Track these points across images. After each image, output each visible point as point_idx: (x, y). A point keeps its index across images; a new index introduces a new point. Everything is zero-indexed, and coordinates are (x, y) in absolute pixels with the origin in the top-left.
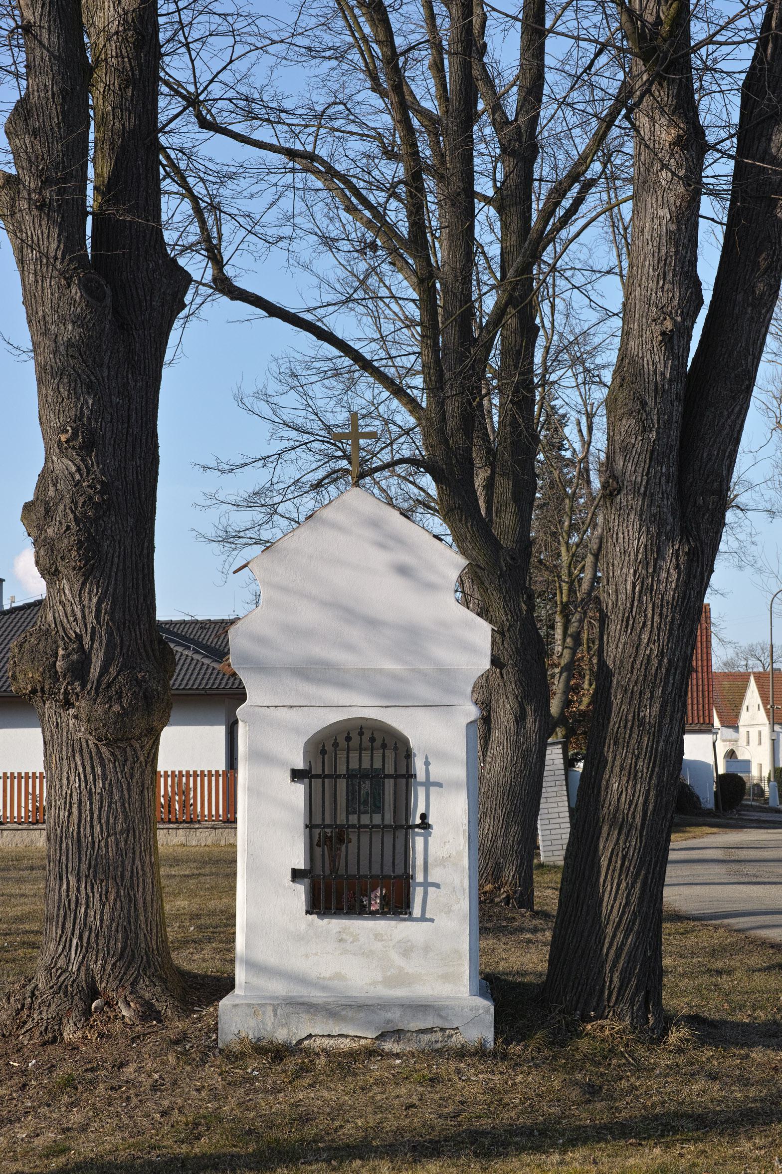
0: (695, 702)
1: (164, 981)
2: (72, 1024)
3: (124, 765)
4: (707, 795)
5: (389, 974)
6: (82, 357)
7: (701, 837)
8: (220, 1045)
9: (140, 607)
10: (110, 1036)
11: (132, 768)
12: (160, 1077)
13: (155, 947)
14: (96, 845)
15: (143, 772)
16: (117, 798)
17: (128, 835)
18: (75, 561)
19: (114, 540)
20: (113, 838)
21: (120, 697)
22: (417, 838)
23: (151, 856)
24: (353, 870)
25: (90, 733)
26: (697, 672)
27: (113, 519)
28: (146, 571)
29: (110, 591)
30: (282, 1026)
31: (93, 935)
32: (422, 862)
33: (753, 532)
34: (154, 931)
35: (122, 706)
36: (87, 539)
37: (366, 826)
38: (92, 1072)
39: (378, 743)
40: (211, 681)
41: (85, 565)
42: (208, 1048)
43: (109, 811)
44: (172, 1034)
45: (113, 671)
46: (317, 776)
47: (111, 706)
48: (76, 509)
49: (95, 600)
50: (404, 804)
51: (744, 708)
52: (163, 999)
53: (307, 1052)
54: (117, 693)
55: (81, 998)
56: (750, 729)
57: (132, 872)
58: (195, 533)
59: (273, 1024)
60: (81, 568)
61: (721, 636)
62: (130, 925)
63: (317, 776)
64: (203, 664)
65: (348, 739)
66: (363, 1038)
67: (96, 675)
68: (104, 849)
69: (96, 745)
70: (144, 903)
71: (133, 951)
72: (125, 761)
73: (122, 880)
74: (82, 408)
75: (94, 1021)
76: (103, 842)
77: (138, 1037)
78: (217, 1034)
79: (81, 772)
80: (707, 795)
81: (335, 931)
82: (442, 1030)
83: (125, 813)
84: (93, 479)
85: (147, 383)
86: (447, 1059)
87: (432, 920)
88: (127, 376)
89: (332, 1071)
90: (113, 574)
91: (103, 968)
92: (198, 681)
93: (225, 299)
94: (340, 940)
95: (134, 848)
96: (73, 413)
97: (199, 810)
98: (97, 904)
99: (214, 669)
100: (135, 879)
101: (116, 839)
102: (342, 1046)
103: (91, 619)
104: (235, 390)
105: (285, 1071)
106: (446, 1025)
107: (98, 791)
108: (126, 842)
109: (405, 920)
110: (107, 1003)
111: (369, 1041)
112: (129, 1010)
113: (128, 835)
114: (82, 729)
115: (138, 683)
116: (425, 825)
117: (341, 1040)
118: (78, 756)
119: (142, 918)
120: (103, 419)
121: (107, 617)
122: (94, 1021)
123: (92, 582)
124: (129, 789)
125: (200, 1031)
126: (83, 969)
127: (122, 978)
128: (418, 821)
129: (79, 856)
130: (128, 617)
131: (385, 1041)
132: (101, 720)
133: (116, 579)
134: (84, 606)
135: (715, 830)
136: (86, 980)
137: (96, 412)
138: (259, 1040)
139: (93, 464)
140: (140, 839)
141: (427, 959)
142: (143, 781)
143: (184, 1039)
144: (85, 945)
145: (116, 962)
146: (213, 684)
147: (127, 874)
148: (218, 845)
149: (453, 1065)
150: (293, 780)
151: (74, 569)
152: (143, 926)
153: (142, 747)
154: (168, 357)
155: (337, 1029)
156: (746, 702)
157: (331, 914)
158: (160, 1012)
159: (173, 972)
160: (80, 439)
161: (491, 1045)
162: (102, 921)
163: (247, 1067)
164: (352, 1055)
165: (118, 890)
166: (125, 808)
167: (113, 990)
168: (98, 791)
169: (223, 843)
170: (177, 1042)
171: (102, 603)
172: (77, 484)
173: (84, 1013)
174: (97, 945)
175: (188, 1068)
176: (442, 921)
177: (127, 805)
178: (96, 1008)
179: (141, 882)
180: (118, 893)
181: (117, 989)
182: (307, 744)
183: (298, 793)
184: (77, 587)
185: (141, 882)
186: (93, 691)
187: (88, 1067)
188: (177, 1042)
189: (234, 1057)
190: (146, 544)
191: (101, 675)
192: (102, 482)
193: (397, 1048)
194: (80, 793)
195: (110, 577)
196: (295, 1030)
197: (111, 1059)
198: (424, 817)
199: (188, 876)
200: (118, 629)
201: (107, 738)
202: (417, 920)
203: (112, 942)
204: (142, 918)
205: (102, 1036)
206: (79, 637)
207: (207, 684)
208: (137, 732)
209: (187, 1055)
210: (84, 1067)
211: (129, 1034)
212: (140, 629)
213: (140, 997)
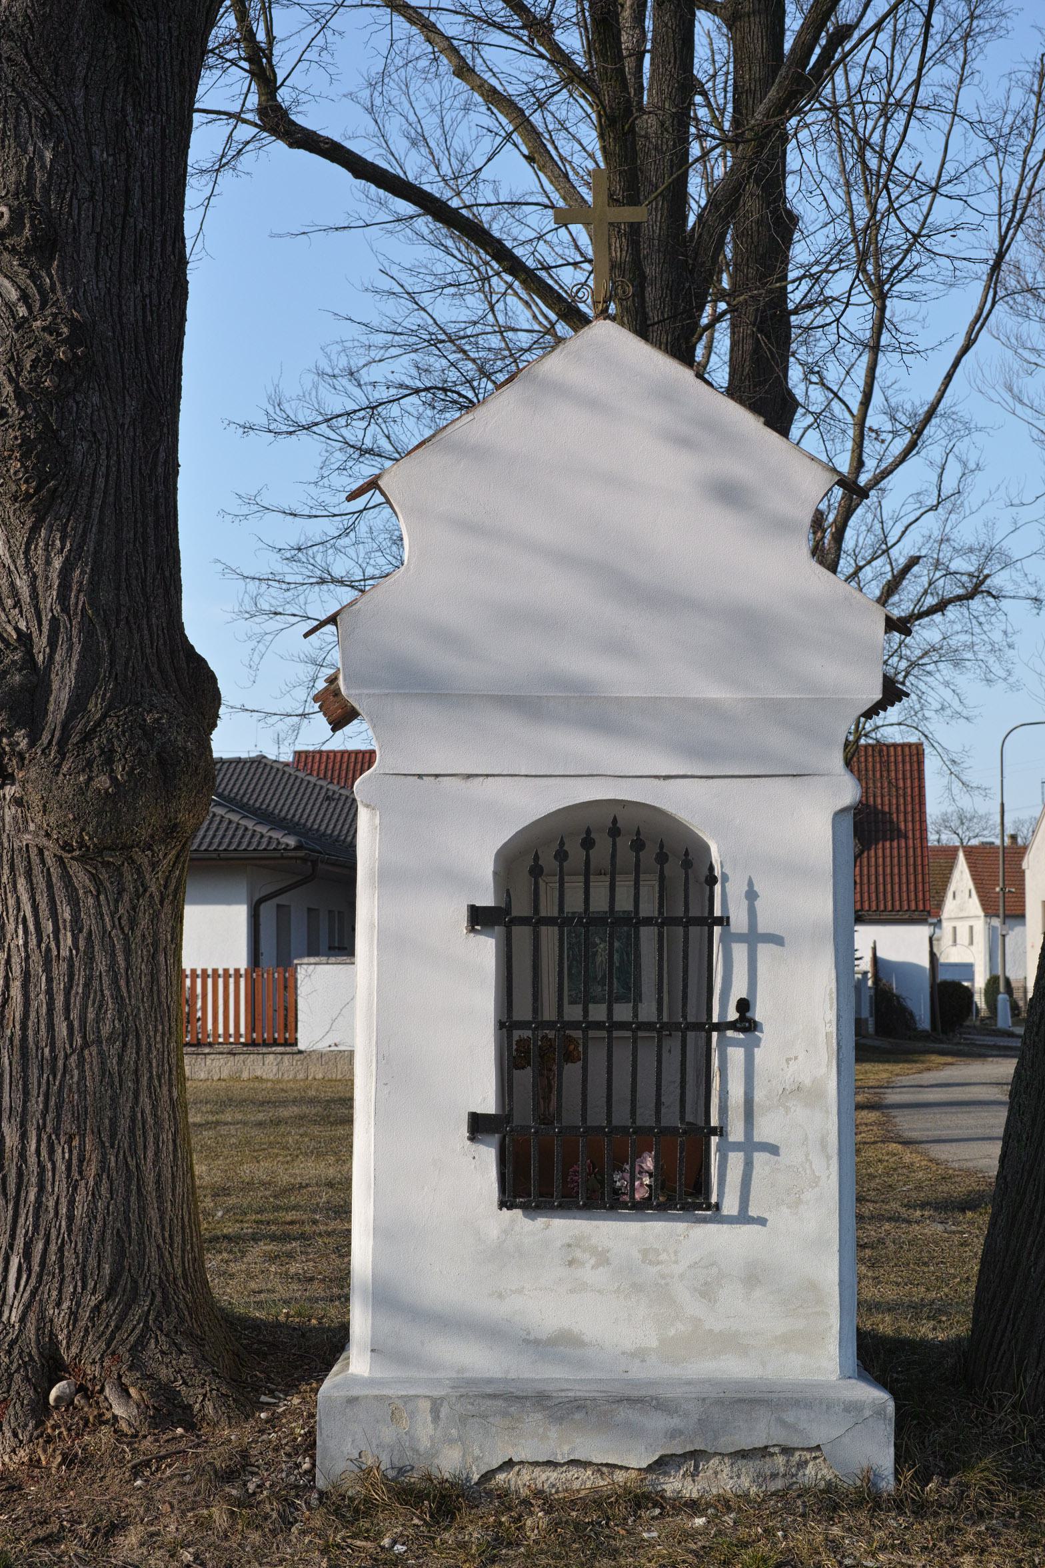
0: (904, 880)
1: (198, 1341)
2: (8, 1434)
3: (117, 901)
4: (922, 1010)
5: (672, 1332)
6: (30, 61)
7: (937, 1069)
8: (321, 1483)
9: (149, 580)
10: (86, 1462)
11: (134, 909)
12: (196, 1557)
13: (180, 1271)
14: (60, 1063)
15: (155, 918)
16: (103, 968)
17: (124, 1045)
18: (17, 482)
19: (96, 440)
20: (94, 1049)
21: (109, 761)
22: (730, 1050)
23: (171, 1086)
24: (597, 1117)
25: (48, 835)
26: (906, 838)
27: (95, 400)
28: (162, 510)
29: (90, 546)
30: (451, 1441)
31: (53, 1248)
32: (741, 1100)
33: (1010, 630)
34: (178, 1239)
35: (113, 779)
36: (40, 437)
37: (623, 1026)
38: (49, 1544)
39: (648, 856)
40: (227, 840)
41: (38, 490)
42: (298, 1496)
43: (86, 996)
44: (218, 1456)
45: (95, 708)
46: (523, 921)
47: (90, 779)
48: (18, 374)
49: (57, 563)
50: (696, 977)
51: (950, 894)
52: (198, 1380)
53: (503, 1494)
54: (102, 752)
55: (27, 1379)
56: (958, 924)
57: (133, 1120)
58: (220, 567)
59: (432, 1438)
60: (28, 497)
61: (964, 778)
62: (129, 1226)
63: (523, 921)
64: (214, 815)
65: (561, 855)
66: (621, 1468)
67: (61, 716)
68: (76, 1072)
69: (60, 860)
70: (158, 1182)
71: (135, 1282)
72: (119, 893)
73: (113, 1136)
74: (30, 167)
75: (54, 1427)
76: (73, 1059)
77: (147, 1464)
78: (313, 1457)
79: (29, 915)
80: (922, 1010)
81: (559, 1244)
82: (787, 1451)
83: (118, 998)
84: (55, 316)
85: (163, 129)
86: (803, 1515)
87: (762, 1221)
88: (123, 109)
89: (562, 1544)
90: (95, 512)
91: (74, 1315)
92: (207, 840)
93: (280, 146)
94: (571, 1263)
95: (136, 1071)
96: (13, 179)
97: (210, 1026)
98: (61, 1186)
99: (230, 822)
100: (139, 1133)
101: (101, 1053)
102: (576, 1485)
103: (49, 600)
104: (271, 390)
105: (463, 1545)
106: (795, 1441)
107: (65, 953)
108: (121, 1058)
109: (705, 1220)
110: (81, 1389)
111: (634, 1474)
112: (127, 1404)
113: (124, 1045)
114: (32, 827)
115: (148, 734)
116: (746, 1023)
117: (574, 1472)
118: (21, 882)
119: (153, 1214)
120: (74, 193)
121: (82, 597)
122: (54, 1427)
123: (51, 526)
124: (128, 952)
125: (276, 1450)
126: (32, 1317)
127: (112, 1338)
128: (733, 1015)
129: (25, 1086)
130: (125, 600)
131: (666, 1474)
132: (71, 808)
133: (101, 522)
134: (35, 577)
135: (949, 1059)
136: (38, 1342)
137: (60, 177)
138: (401, 1471)
139: (53, 284)
140: (149, 1051)
141: (749, 1301)
142: (156, 934)
143: (243, 1467)
144: (36, 1268)
145: (101, 1302)
146: (230, 843)
147: (124, 1124)
148: (238, 1079)
149: (818, 1531)
150: (472, 929)
151: (15, 499)
152: (156, 1229)
153: (154, 865)
154: (190, 229)
155: (566, 1448)
156: (952, 887)
157: (552, 1208)
158: (190, 1407)
159: (216, 1319)
160: (27, 232)
161: (888, 1484)
162: (71, 1218)
163: (380, 1535)
164: (600, 1505)
165: (104, 1155)
166: (118, 988)
167: (94, 1362)
168: (65, 953)
169: (245, 1075)
170: (229, 1476)
171: (73, 570)
172: (21, 324)
173: (33, 1410)
174: (62, 1269)
175: (255, 1537)
176: (780, 1218)
177: (122, 983)
178: (58, 1399)
179: (151, 1139)
180: (103, 1161)
181: (102, 1359)
182: (499, 854)
183: (484, 950)
184: (21, 536)
185: (151, 1139)
186: (54, 748)
187: (41, 1532)
188: (229, 1476)
189: (350, 1510)
190: (162, 455)
191: (71, 715)
192: (72, 322)
193: (691, 1490)
194: (28, 957)
195: (88, 517)
196: (477, 1452)
197: (90, 1513)
198: (744, 1006)
199: (200, 1125)
200: (106, 624)
201: (82, 844)
202: (730, 1220)
203: (92, 1262)
204: (153, 1214)
205: (72, 1462)
206: (25, 639)
207: (220, 844)
208: (144, 834)
209: (251, 1506)
210: (32, 1535)
211: (128, 1456)
212: (150, 627)
213: (150, 1377)
